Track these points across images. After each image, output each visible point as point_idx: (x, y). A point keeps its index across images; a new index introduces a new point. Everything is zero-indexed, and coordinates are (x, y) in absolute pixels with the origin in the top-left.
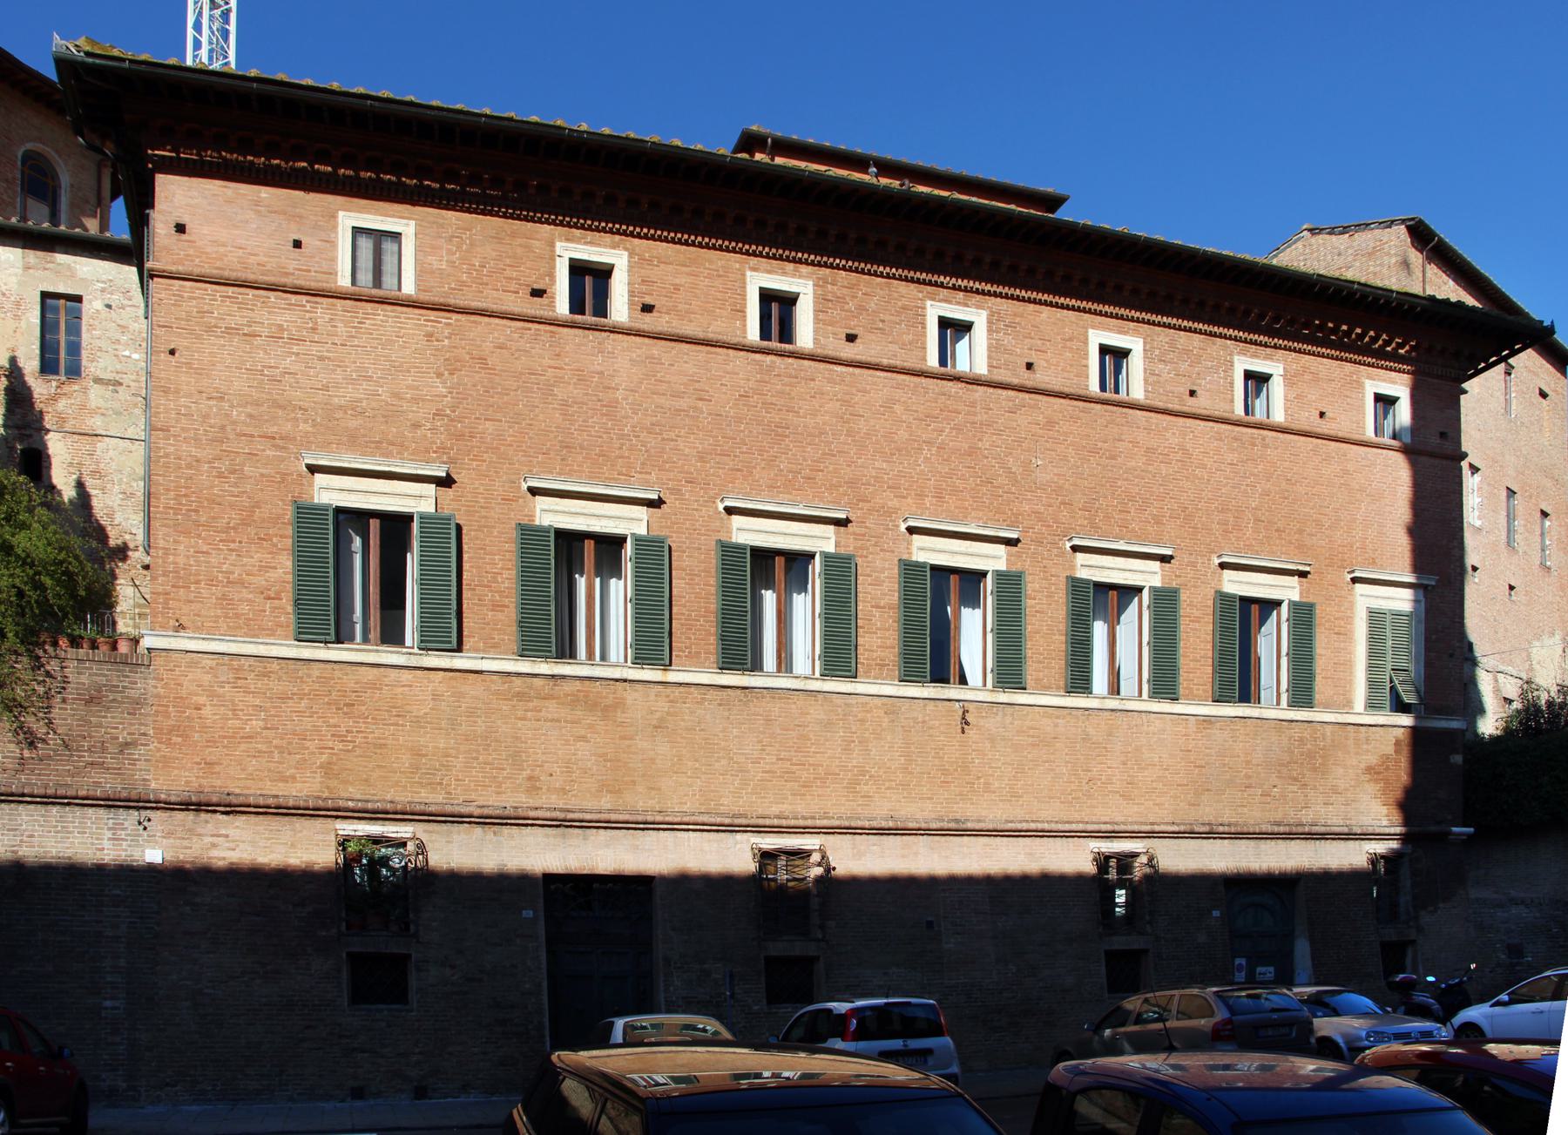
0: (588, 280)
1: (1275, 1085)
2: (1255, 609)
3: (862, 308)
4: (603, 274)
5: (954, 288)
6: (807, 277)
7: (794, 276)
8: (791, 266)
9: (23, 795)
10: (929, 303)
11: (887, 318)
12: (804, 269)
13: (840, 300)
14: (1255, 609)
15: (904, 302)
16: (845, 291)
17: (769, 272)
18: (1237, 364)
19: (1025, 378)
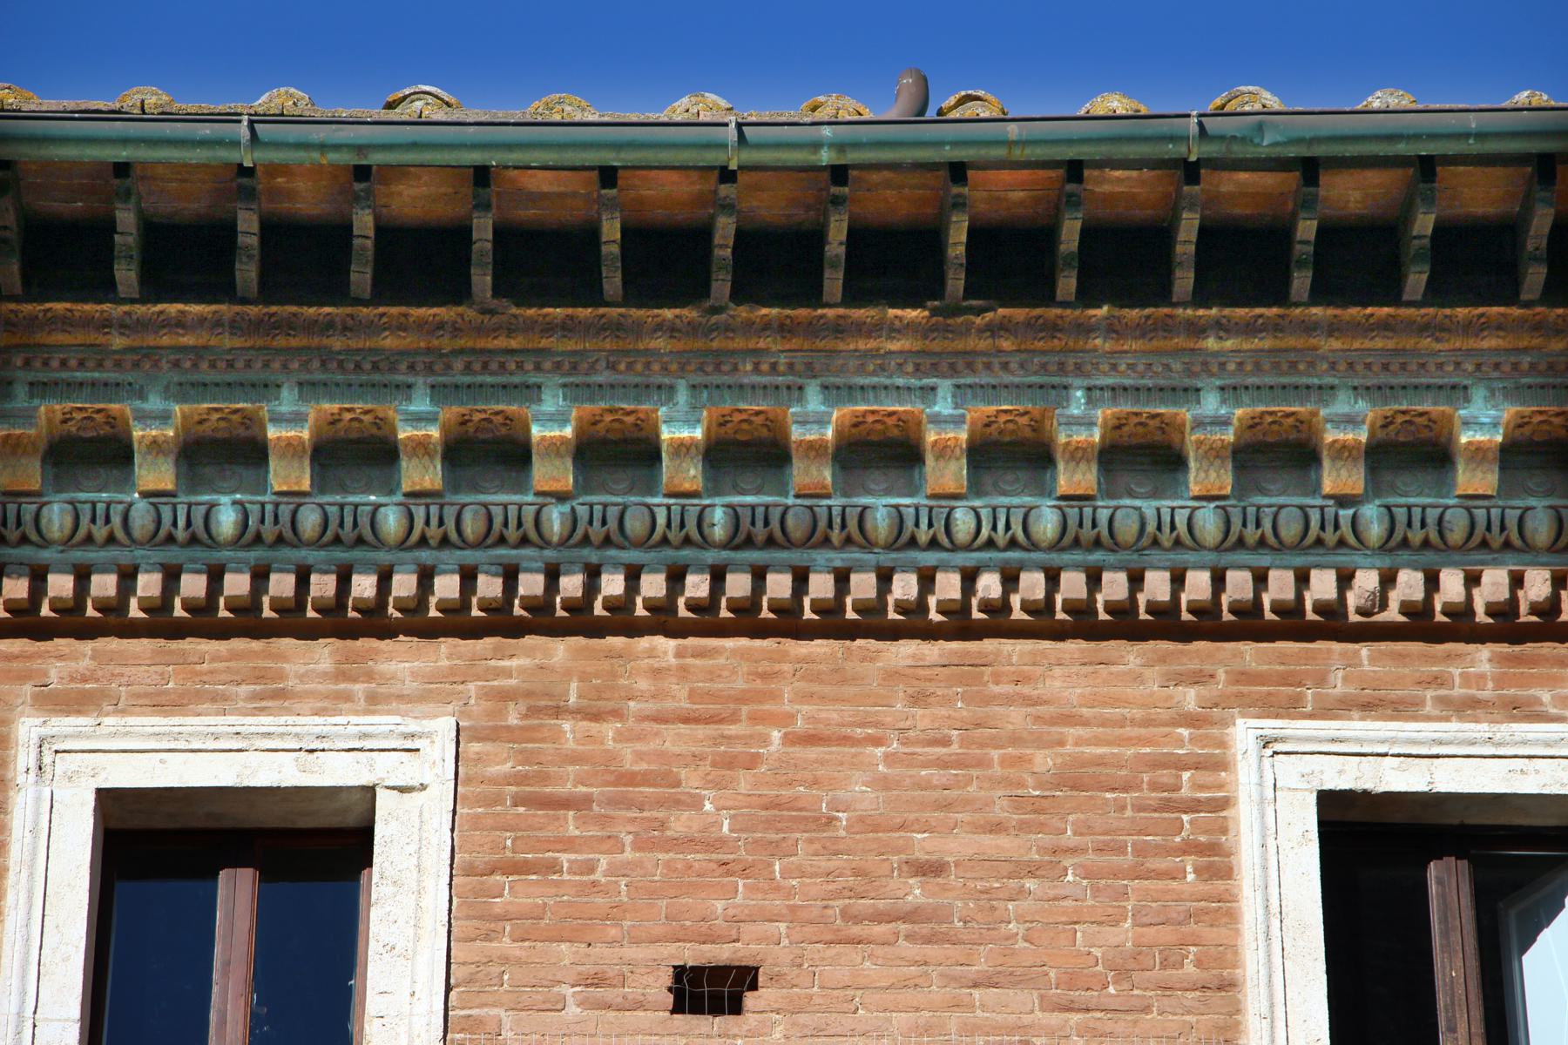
0: (236, 895)
1: (1462, 130)
2: (1446, 886)
3: (782, 818)
4: (318, 851)
5: (1420, 625)
6: (428, 695)
7: (335, 702)
8: (324, 653)
9: (1264, 828)
10: (1244, 732)
11: (956, 846)
12: (401, 659)
13: (642, 791)
14: (1446, 886)
15: (1078, 744)
16: (674, 739)
17: (162, 704)
18: (1248, 774)
19: (856, 118)
